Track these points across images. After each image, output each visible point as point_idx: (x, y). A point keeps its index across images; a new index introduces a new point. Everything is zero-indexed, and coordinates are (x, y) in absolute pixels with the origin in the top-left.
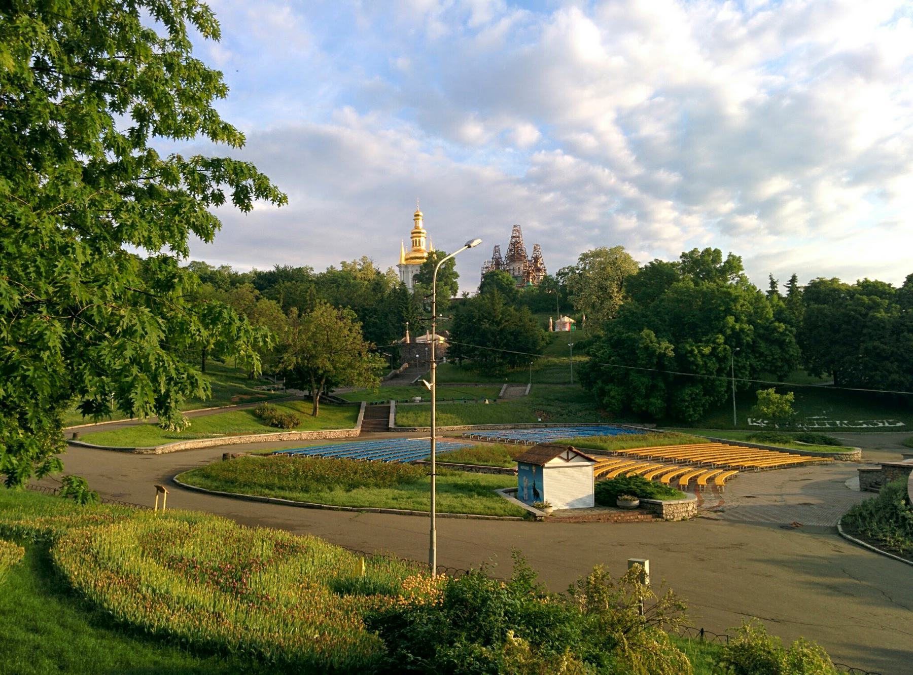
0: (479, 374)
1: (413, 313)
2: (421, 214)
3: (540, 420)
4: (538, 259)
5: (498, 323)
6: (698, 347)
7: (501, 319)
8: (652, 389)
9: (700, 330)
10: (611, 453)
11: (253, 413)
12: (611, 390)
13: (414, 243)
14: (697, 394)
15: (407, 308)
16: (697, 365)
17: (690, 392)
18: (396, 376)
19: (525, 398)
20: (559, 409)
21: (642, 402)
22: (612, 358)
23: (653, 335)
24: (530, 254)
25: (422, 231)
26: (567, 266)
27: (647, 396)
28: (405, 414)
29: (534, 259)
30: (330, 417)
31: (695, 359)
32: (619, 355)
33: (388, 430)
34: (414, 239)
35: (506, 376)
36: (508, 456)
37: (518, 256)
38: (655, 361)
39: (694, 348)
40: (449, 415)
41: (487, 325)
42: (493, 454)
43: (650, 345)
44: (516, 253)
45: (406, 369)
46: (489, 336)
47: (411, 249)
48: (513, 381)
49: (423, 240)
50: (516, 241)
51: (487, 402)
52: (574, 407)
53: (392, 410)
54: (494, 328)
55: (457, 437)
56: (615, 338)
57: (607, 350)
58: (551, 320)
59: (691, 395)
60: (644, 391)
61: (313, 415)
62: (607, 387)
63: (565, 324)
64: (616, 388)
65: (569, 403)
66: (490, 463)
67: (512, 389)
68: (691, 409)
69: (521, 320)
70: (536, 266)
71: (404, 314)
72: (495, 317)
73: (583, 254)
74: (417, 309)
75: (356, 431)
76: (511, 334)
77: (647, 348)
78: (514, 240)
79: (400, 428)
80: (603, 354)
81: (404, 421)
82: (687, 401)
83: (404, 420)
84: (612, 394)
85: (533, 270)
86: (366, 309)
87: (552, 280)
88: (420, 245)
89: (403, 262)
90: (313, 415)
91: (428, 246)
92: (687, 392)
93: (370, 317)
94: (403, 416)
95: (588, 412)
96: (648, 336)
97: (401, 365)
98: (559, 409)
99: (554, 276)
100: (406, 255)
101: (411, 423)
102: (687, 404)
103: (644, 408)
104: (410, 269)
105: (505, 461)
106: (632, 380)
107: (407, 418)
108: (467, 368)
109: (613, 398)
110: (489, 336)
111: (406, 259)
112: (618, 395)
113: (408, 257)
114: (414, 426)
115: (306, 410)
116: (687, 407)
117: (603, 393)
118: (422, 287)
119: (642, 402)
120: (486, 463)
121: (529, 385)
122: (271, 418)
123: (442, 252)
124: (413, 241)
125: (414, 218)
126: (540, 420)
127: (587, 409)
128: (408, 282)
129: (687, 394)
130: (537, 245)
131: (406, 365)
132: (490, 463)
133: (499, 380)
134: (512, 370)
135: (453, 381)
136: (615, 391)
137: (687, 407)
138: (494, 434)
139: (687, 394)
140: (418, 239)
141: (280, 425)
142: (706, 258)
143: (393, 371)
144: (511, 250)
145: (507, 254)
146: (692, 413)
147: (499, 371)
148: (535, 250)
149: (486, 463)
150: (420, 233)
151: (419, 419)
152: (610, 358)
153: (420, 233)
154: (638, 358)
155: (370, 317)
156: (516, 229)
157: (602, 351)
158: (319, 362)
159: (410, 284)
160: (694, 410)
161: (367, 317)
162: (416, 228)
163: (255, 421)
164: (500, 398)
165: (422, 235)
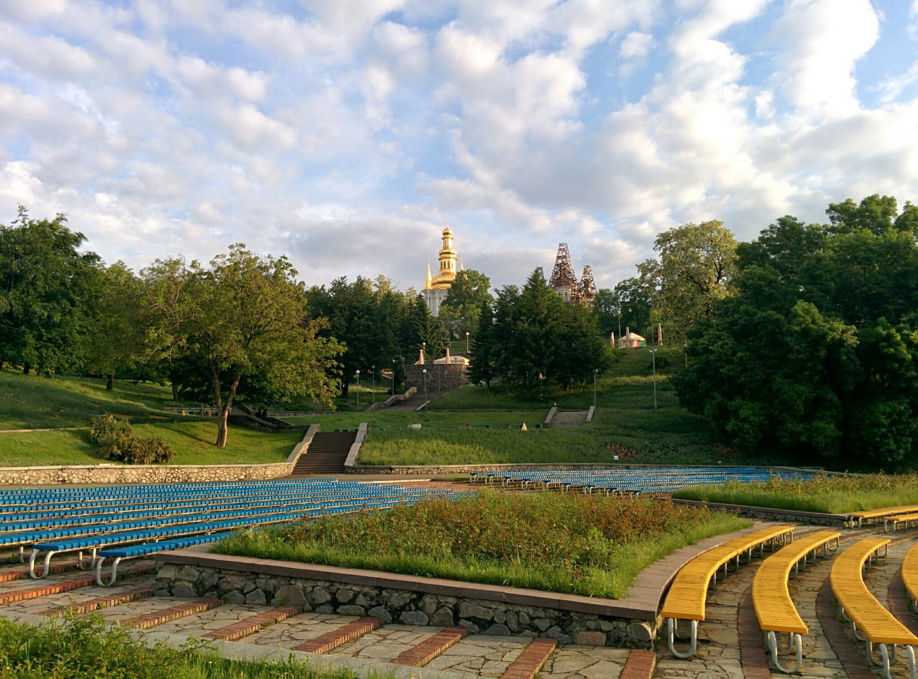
0: (514, 398)
1: (432, 333)
2: (450, 232)
3: (616, 458)
4: (589, 282)
5: (542, 324)
6: (899, 330)
7: (546, 318)
8: (815, 406)
9: (890, 307)
10: (843, 519)
11: (86, 437)
12: (741, 408)
13: (443, 266)
14: (900, 414)
15: (424, 326)
16: (901, 361)
17: (888, 410)
18: (397, 403)
19: (587, 425)
20: (646, 442)
21: (800, 428)
22: (739, 354)
23: (815, 310)
24: (579, 276)
25: (452, 251)
26: (629, 278)
27: (807, 418)
28: (378, 444)
29: (585, 283)
30: (248, 448)
31: (895, 349)
32: (748, 349)
33: (342, 469)
34: (443, 261)
35: (554, 399)
36: (595, 531)
37: (565, 279)
38: (823, 353)
39: (893, 331)
40: (457, 447)
41: (526, 325)
42: (532, 521)
43: (813, 326)
44: (562, 274)
45: (414, 394)
46: (529, 340)
47: (439, 273)
48: (564, 407)
49: (452, 261)
50: (563, 262)
51: (525, 428)
52: (672, 439)
53: (360, 437)
54: (536, 329)
55: (458, 481)
56: (742, 321)
57: (730, 342)
58: (613, 337)
59: (889, 416)
60: (802, 408)
61: (216, 445)
62: (733, 403)
63: (631, 341)
64: (750, 404)
65: (662, 434)
66: (516, 569)
67: (565, 414)
68: (891, 441)
69: (575, 319)
70: (587, 291)
71: (421, 333)
72: (537, 314)
73: (662, 235)
74: (437, 327)
75: (285, 468)
76: (563, 337)
77: (805, 333)
78: (560, 261)
79: (365, 467)
80: (722, 347)
81: (375, 455)
82: (883, 426)
83: (376, 453)
84: (743, 413)
85: (583, 295)
86: (356, 308)
87: (610, 294)
88: (449, 267)
89: (430, 287)
90: (216, 445)
91: (458, 266)
92: (882, 411)
93: (359, 318)
94: (375, 447)
95: (696, 447)
96: (808, 312)
97: (407, 389)
98: (646, 442)
99: (612, 289)
100: (433, 280)
101: (385, 458)
102: (884, 430)
103: (803, 439)
104: (437, 295)
105: (585, 559)
106: (779, 390)
107: (381, 450)
108: (495, 390)
109: (745, 420)
110: (529, 340)
111: (433, 284)
112: (754, 415)
113: (436, 281)
114: (390, 462)
115: (207, 437)
116: (884, 436)
117: (724, 414)
118: (449, 310)
119: (800, 428)
120: (492, 570)
121: (592, 408)
122: (109, 445)
123: (475, 272)
124: (442, 263)
125: (443, 236)
126: (616, 458)
127: (695, 443)
128: (434, 308)
129: (884, 413)
130: (588, 266)
131: (413, 390)
132: (516, 569)
133: (544, 405)
134: (563, 393)
135: (477, 407)
136: (747, 409)
137: (884, 436)
138: (539, 475)
139: (884, 413)
140: (447, 260)
141: (125, 457)
142: (874, 207)
143: (394, 396)
144: (556, 273)
145: (552, 277)
146: (893, 446)
147: (544, 392)
148: (585, 272)
149: (492, 570)
150: (449, 253)
151: (402, 451)
152: (734, 354)
153: (449, 253)
154: (790, 350)
155: (359, 318)
156: (563, 248)
157: (720, 343)
158: (221, 349)
159: (434, 308)
160: (896, 442)
161: (356, 318)
162: (446, 247)
163: (82, 449)
164: (546, 426)
165: (451, 256)
